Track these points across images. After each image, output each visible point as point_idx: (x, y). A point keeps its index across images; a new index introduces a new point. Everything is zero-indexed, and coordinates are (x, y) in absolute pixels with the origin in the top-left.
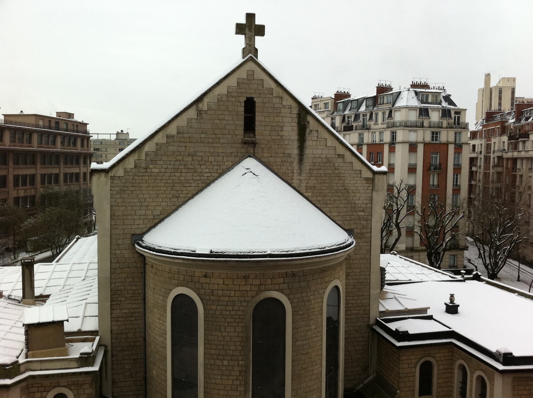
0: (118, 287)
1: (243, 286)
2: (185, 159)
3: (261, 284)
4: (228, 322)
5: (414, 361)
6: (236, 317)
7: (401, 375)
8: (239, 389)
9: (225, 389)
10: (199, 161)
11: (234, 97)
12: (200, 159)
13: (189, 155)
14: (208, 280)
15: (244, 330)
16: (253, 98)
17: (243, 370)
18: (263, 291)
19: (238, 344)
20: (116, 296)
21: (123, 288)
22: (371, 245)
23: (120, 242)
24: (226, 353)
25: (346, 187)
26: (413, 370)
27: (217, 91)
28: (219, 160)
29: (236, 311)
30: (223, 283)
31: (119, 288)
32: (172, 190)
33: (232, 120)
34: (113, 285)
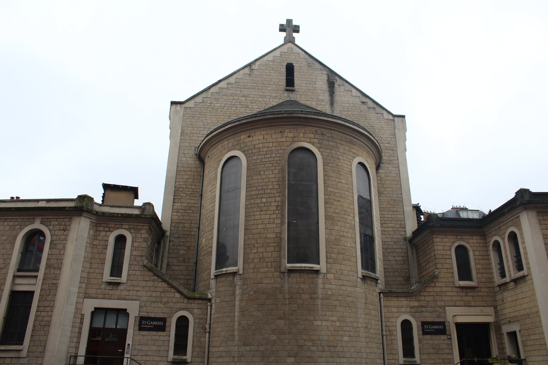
0: (181, 185)
1: (280, 138)
3: (294, 137)
5: (448, 244)
7: (438, 256)
8: (276, 222)
9: (263, 223)
11: (278, 62)
13: (243, 96)
14: (251, 139)
15: (280, 172)
16: (292, 63)
18: (297, 142)
20: (178, 192)
21: (185, 186)
22: (399, 170)
23: (186, 152)
24: (265, 192)
26: (448, 253)
27: (266, 58)
28: (266, 100)
32: (229, 118)
33: (277, 76)
34: (177, 183)
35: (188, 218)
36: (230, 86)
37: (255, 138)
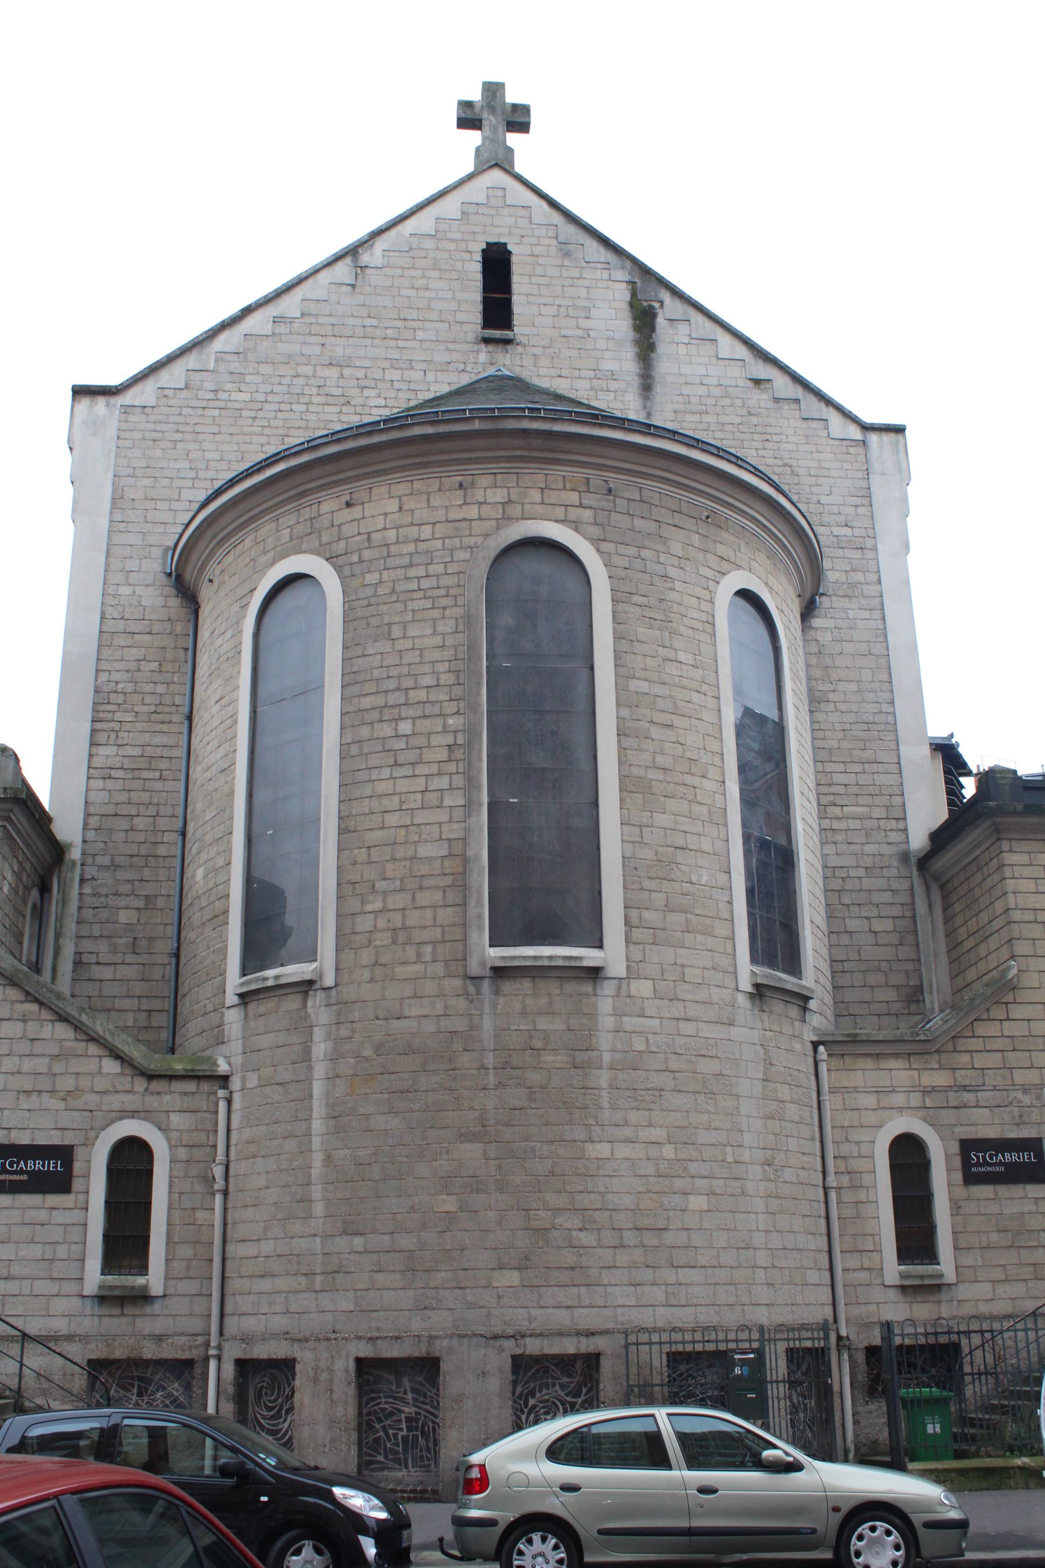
0: (117, 683)
1: (458, 508)
3: (510, 501)
4: (413, 610)
8: (448, 801)
9: (404, 807)
10: (358, 379)
11: (452, 241)
12: (361, 373)
14: (356, 512)
17: (460, 741)
19: (442, 667)
20: (109, 707)
21: (130, 688)
22: (884, 619)
23: (133, 565)
24: (407, 699)
25: (786, 461)
27: (409, 226)
28: (413, 379)
29: (437, 576)
30: (401, 508)
31: (120, 686)
34: (103, 677)
35: (145, 797)
36: (282, 329)
37: (370, 509)
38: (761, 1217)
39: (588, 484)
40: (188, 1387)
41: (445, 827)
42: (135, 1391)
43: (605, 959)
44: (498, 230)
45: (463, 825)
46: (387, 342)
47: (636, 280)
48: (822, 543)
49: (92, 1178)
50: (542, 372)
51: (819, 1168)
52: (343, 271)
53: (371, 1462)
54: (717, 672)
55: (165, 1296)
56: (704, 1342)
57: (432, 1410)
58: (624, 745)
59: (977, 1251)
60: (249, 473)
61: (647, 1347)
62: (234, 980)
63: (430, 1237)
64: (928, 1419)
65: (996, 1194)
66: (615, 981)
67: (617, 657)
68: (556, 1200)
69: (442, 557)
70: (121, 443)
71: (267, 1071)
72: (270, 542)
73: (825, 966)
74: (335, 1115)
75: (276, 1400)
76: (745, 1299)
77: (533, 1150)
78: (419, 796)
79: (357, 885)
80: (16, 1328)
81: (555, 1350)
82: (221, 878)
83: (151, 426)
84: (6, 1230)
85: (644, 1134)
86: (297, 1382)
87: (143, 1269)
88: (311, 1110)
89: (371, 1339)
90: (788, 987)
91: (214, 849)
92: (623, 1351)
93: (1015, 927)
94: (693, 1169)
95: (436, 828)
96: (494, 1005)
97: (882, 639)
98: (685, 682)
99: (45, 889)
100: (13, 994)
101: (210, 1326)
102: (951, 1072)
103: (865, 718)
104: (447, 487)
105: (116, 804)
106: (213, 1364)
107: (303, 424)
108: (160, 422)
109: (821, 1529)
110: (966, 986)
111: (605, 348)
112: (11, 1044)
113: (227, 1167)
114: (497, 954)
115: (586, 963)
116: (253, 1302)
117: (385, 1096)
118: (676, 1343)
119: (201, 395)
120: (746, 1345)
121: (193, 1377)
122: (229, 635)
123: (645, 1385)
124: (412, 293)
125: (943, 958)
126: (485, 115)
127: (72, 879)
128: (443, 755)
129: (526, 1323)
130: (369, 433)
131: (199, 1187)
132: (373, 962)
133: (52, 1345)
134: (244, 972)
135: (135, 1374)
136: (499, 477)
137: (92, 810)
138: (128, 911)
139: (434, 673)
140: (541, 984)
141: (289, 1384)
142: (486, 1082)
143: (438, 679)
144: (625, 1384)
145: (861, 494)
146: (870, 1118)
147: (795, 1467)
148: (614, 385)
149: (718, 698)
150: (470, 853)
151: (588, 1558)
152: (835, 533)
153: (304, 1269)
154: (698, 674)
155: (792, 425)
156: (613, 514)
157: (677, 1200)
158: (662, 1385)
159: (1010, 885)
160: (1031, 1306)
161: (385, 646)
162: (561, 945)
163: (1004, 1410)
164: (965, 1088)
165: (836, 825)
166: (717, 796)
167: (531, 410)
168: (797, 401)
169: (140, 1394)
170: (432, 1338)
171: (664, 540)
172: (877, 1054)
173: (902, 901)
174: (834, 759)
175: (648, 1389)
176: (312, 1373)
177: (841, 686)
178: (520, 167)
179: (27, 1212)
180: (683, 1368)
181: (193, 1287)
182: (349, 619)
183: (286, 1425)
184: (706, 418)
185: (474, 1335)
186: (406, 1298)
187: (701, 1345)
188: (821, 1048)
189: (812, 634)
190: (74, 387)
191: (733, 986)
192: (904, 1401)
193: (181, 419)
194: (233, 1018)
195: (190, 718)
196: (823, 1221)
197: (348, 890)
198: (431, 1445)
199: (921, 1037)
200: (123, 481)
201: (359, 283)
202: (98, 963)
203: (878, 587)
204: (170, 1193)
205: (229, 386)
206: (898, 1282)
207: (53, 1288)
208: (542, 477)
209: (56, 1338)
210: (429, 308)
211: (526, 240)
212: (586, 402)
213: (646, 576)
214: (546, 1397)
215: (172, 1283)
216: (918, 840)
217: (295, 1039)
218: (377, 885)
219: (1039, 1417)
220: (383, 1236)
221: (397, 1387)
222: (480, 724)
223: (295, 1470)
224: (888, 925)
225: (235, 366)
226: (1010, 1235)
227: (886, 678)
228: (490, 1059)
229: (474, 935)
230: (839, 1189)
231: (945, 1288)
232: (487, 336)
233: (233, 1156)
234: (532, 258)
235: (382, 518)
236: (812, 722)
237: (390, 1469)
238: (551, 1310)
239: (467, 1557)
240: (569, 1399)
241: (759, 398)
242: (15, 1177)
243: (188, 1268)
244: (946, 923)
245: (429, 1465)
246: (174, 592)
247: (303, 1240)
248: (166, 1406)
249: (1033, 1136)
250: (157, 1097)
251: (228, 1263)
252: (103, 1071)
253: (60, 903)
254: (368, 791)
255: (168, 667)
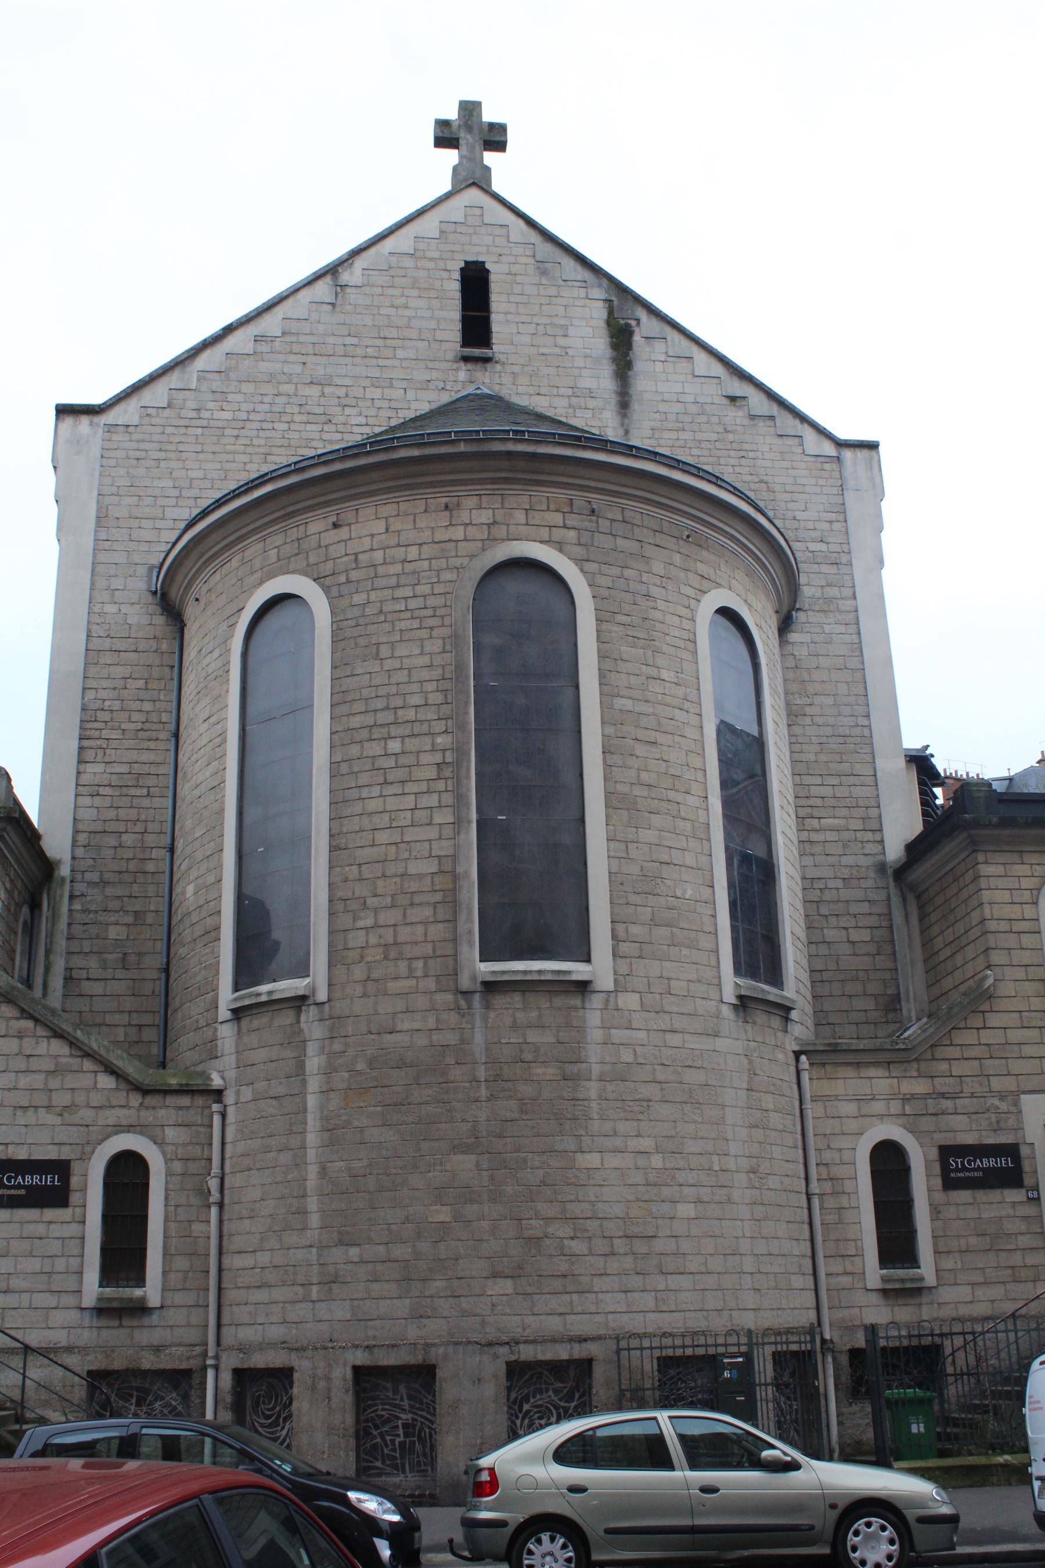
2: (301, 393)
3: (495, 522)
4: (401, 630)
6: (424, 612)
8: (437, 820)
10: (339, 397)
11: (431, 259)
12: (341, 392)
14: (343, 533)
17: (449, 759)
19: (430, 687)
20: (96, 725)
22: (859, 633)
23: (117, 583)
24: (396, 718)
27: (388, 245)
28: (394, 397)
30: (387, 529)
31: (107, 703)
34: (90, 695)
35: (133, 814)
36: (263, 348)
38: (747, 1224)
39: (571, 505)
40: (185, 1397)
41: (435, 845)
42: (134, 1401)
43: (593, 973)
44: (476, 249)
45: (452, 842)
46: (367, 360)
47: (613, 298)
48: (798, 559)
49: (89, 1191)
50: (521, 389)
51: (802, 1175)
52: (323, 290)
53: (370, 1468)
54: (698, 689)
55: (162, 1307)
56: (693, 1346)
57: (429, 1416)
58: (609, 762)
59: (957, 1255)
60: (235, 494)
61: (639, 1352)
62: (226, 996)
63: (424, 1246)
64: (912, 1419)
65: (975, 1199)
66: (603, 995)
67: (602, 676)
68: (547, 1210)
69: (429, 578)
70: (105, 462)
71: (261, 1085)
72: (257, 563)
73: (805, 977)
74: (330, 1128)
75: (274, 1408)
76: (732, 1304)
77: (525, 1161)
78: (409, 814)
79: (348, 902)
80: (18, 1341)
81: (548, 1356)
82: (212, 895)
83: (134, 445)
84: (5, 1244)
85: (633, 1144)
86: (295, 1391)
87: (140, 1280)
88: (306, 1123)
89: (367, 1347)
90: (771, 998)
91: (204, 866)
92: (615, 1358)
93: (990, 937)
94: (681, 1176)
95: (426, 845)
96: (485, 1019)
97: (857, 653)
98: (668, 699)
99: (35, 906)
100: (7, 1010)
101: (207, 1337)
102: (930, 1080)
103: (841, 731)
104: (433, 509)
105: (104, 821)
106: (210, 1374)
107: (285, 442)
108: (143, 441)
109: (818, 1526)
110: (942, 995)
111: (582, 365)
112: (7, 1061)
113: (222, 1180)
114: (487, 969)
115: (574, 977)
116: (250, 1313)
117: (379, 1109)
118: (666, 1348)
119: (184, 413)
120: (735, 1349)
121: (191, 1387)
122: (216, 653)
123: (638, 1389)
124: (391, 311)
125: (920, 967)
126: (462, 134)
127: (61, 896)
128: (432, 773)
129: (520, 1330)
130: (356, 456)
131: (195, 1200)
132: (365, 978)
133: (52, 1356)
134: (236, 988)
135: (134, 1384)
136: (484, 498)
137: (81, 827)
138: (118, 927)
139: (422, 692)
140: (531, 998)
141: (287, 1393)
142: (477, 1094)
143: (426, 699)
144: (617, 1388)
145: (835, 510)
146: (851, 1125)
147: (793, 1466)
148: (592, 403)
149: (700, 715)
150: (459, 869)
151: (596, 1557)
152: (811, 549)
153: (301, 1279)
154: (680, 691)
155: (767, 442)
156: (596, 534)
157: (666, 1208)
158: (653, 1389)
159: (986, 895)
160: (1009, 1308)
161: (374, 666)
162: (550, 959)
163: (984, 1410)
164: (943, 1096)
165: (814, 837)
166: (701, 812)
167: (515, 432)
168: (772, 418)
169: (139, 1404)
170: (428, 1346)
171: (647, 559)
172: (858, 1063)
173: (879, 911)
174: (811, 772)
175: (640, 1393)
176: (309, 1381)
177: (817, 700)
178: (497, 186)
179: (26, 1226)
180: (672, 1372)
181: (190, 1298)
182: (337, 638)
183: (284, 1432)
184: (683, 436)
185: (469, 1342)
186: (403, 1307)
187: (691, 1350)
188: (803, 1058)
189: (789, 648)
190: (57, 406)
191: (718, 998)
192: (888, 1401)
193: (164, 438)
194: (226, 1033)
195: (176, 735)
196: (806, 1227)
197: (339, 906)
198: (427, 1450)
199: (901, 1046)
200: (107, 500)
201: (339, 302)
202: (88, 979)
203: (854, 602)
204: (166, 1206)
205: (211, 405)
206: (879, 1286)
207: (50, 1300)
208: (526, 499)
209: (55, 1350)
210: (408, 327)
211: (504, 259)
212: (564, 420)
213: (629, 596)
214: (540, 1402)
215: (170, 1294)
216: (894, 851)
217: (288, 1053)
218: (369, 902)
219: (1024, 1415)
220: (378, 1247)
221: (394, 1394)
222: (469, 743)
223: (309, 1476)
224: (865, 935)
225: (217, 385)
226: (988, 1239)
227: (862, 692)
228: (481, 1073)
229: (464, 949)
230: (821, 1195)
231: (925, 1292)
232: (466, 354)
233: (227, 1169)
234: (510, 277)
235: (368, 539)
236: (790, 735)
237: (388, 1474)
238: (543, 1317)
239: (477, 1557)
240: (562, 1404)
241: (735, 416)
242: (13, 1192)
243: (185, 1278)
244: (922, 932)
245: (426, 1471)
246: (159, 610)
247: (300, 1250)
248: (165, 1415)
249: (1009, 1141)
250: (152, 1112)
251: (225, 1274)
252: (99, 1086)
253: (50, 920)
254: (358, 808)
255: (154, 685)
